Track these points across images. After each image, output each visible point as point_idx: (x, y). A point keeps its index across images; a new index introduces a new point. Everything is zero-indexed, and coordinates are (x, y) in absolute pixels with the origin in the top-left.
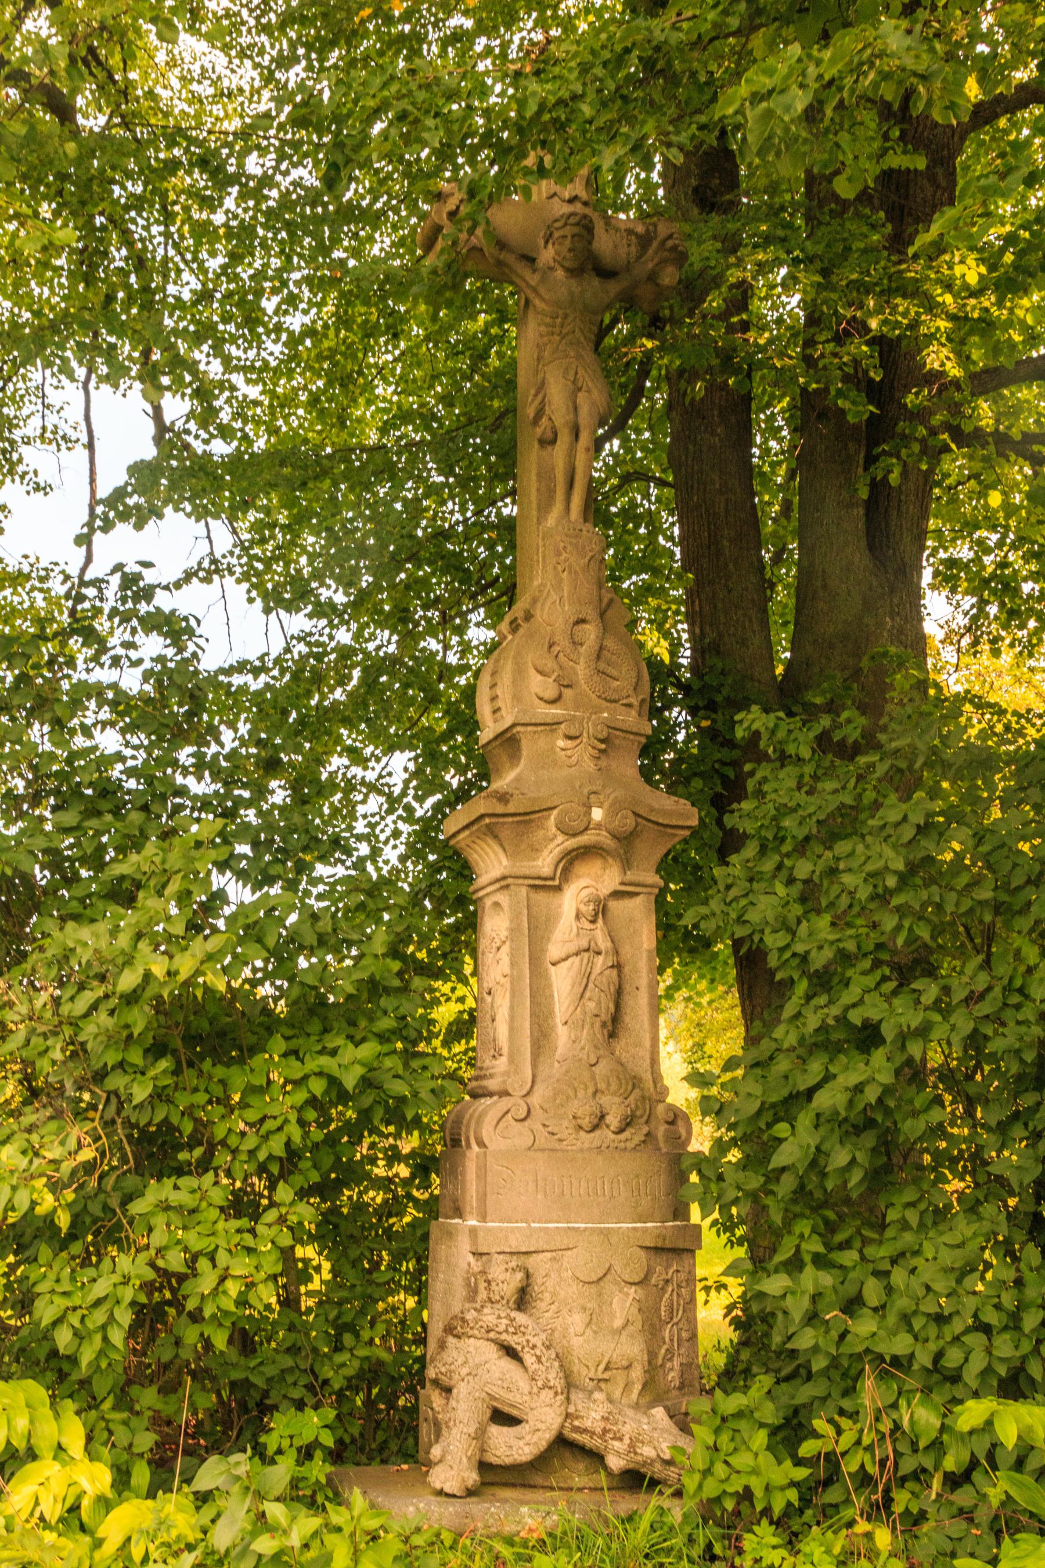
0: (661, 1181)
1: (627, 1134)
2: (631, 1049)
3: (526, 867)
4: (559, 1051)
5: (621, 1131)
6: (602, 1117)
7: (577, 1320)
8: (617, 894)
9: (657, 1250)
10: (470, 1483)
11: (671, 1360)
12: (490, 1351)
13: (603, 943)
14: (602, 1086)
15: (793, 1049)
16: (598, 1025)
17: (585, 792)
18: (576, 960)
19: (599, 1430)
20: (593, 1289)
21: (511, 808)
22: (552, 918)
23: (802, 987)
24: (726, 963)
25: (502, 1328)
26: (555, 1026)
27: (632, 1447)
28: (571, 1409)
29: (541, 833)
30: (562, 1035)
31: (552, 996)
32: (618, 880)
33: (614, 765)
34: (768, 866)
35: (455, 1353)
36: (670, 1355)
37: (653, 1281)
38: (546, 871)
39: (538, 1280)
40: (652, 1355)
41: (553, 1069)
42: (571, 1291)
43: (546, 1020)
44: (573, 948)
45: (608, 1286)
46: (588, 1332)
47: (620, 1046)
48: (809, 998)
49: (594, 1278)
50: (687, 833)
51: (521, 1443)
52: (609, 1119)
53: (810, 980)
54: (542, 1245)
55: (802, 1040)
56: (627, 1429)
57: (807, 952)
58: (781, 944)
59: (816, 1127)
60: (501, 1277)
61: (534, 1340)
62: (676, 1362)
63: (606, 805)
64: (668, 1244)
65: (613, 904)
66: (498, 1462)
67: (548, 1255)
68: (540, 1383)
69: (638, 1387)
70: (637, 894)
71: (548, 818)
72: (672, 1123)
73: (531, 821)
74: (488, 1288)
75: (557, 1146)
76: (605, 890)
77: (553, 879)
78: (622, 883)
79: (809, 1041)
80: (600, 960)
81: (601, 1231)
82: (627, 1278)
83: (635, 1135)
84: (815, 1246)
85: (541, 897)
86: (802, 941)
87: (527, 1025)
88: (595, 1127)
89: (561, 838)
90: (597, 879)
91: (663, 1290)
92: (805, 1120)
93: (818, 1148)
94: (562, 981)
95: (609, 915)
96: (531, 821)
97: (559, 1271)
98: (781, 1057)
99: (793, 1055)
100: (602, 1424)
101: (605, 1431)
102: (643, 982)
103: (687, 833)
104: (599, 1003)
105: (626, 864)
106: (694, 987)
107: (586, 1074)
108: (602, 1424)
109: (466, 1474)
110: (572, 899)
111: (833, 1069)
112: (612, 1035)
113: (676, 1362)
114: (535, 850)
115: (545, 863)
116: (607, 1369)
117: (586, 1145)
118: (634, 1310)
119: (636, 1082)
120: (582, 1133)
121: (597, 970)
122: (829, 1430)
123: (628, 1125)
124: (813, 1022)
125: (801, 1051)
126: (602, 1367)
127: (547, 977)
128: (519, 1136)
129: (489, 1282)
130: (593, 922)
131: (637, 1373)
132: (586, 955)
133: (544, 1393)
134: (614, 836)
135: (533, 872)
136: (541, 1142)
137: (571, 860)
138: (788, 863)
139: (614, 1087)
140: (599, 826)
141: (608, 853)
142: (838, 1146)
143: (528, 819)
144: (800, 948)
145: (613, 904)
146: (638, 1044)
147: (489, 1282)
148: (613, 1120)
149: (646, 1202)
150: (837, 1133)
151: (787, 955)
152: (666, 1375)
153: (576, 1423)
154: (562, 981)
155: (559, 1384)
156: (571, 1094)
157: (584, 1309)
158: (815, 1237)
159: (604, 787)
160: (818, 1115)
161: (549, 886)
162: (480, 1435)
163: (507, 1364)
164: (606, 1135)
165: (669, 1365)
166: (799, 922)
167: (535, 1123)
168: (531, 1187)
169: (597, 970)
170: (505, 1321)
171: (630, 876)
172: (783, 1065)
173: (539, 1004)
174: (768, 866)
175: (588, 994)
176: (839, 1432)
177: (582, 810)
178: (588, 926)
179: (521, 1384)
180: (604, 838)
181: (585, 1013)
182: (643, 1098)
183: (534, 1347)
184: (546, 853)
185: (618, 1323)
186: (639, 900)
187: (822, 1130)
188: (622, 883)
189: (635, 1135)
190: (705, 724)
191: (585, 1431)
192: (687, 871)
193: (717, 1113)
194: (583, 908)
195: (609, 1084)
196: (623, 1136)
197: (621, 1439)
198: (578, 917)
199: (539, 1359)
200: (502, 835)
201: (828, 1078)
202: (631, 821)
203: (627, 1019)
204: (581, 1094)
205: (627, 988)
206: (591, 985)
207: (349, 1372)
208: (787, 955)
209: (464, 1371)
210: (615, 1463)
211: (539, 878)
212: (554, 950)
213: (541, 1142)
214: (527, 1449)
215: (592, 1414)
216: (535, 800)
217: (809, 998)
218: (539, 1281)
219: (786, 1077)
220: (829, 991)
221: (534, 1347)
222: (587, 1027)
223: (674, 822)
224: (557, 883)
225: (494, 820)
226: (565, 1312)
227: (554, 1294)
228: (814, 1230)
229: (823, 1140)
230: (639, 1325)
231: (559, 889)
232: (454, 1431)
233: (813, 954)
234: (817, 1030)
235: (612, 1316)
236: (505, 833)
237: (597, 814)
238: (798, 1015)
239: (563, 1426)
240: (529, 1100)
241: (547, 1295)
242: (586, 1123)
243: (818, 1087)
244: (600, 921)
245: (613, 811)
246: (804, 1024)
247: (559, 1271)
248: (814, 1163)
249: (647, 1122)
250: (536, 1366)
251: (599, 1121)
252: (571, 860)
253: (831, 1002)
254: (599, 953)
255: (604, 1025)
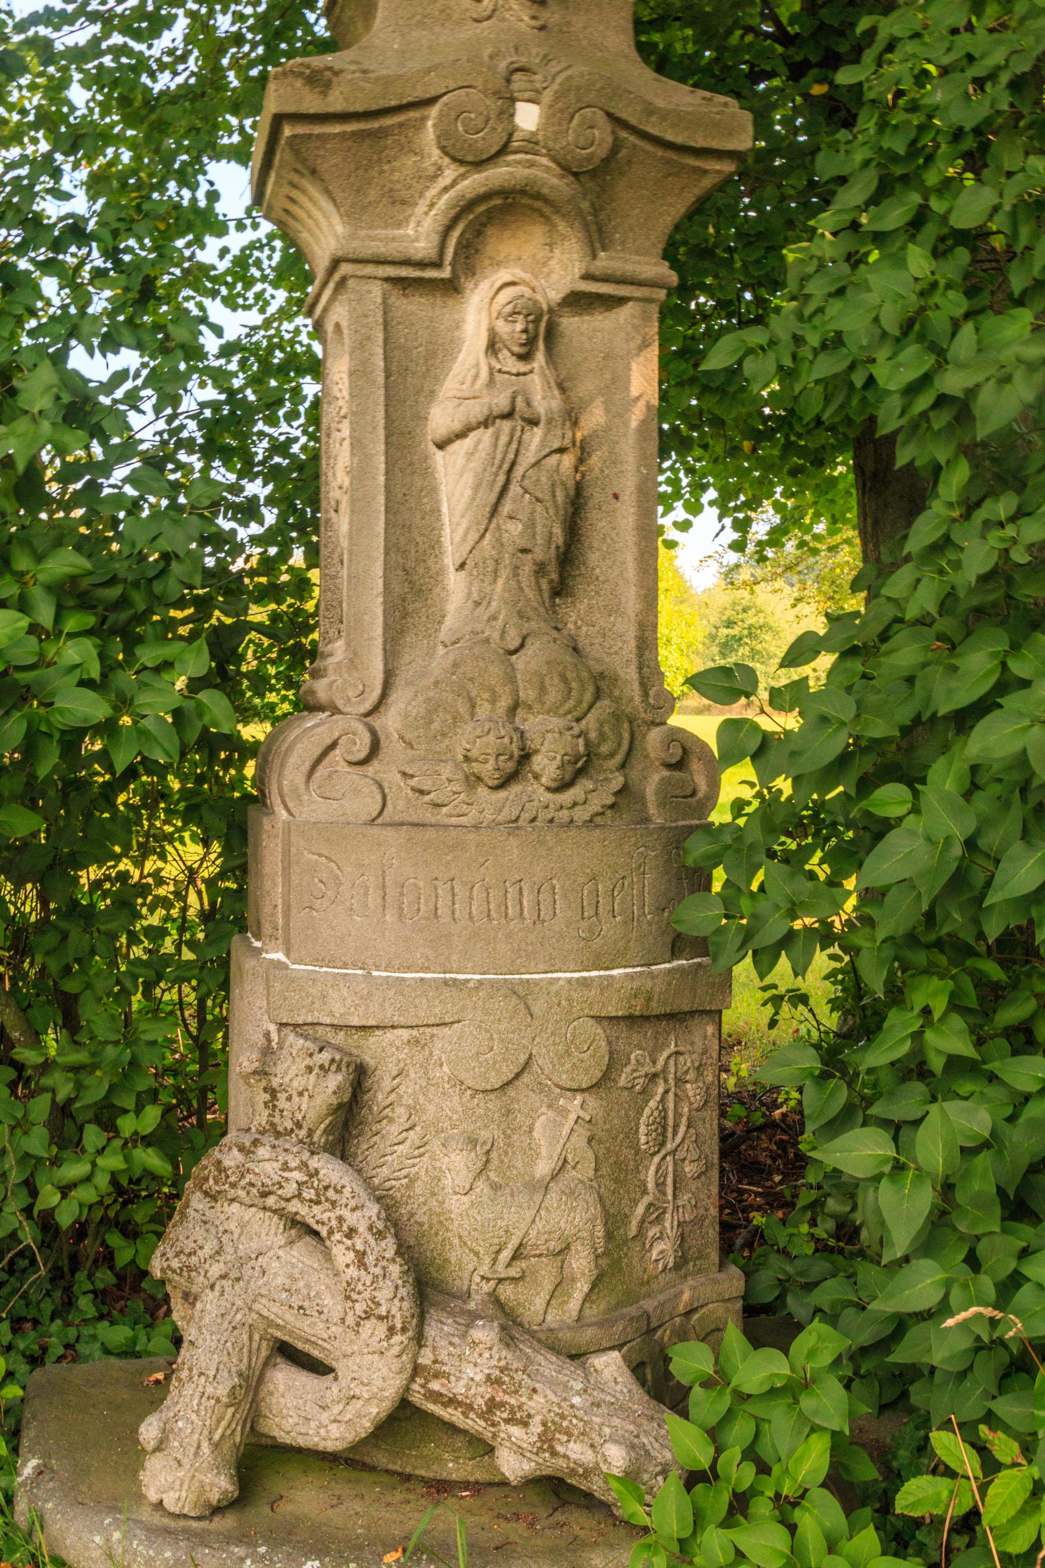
0: (650, 882)
1: (575, 793)
2: (600, 619)
3: (379, 240)
4: (449, 622)
5: (562, 786)
6: (525, 757)
7: (456, 1165)
8: (578, 301)
9: (631, 1020)
10: (214, 1497)
11: (659, 1220)
12: (268, 1232)
13: (543, 399)
14: (528, 694)
15: (923, 621)
16: (527, 570)
17: (502, 65)
18: (485, 436)
19: (480, 1402)
20: (494, 1103)
21: (336, 102)
22: (439, 353)
23: (957, 478)
24: (848, 493)
25: (291, 1189)
26: (441, 571)
27: (547, 1442)
28: (426, 1358)
29: (410, 161)
30: (456, 587)
31: (436, 511)
32: (578, 269)
33: (578, 22)
34: (895, 215)
35: (199, 1233)
36: (655, 1213)
37: (622, 1081)
38: (423, 246)
39: (382, 1085)
40: (613, 1222)
41: (431, 660)
42: (449, 1106)
43: (422, 560)
44: (476, 410)
45: (524, 1096)
46: (481, 1185)
47: (575, 614)
48: (970, 506)
49: (495, 1080)
50: (728, 167)
51: (325, 1417)
52: (538, 762)
53: (976, 465)
54: (390, 1015)
55: (948, 601)
56: (539, 1405)
57: (972, 393)
58: (911, 375)
59: (967, 795)
60: (297, 1084)
61: (352, 1219)
62: (669, 1223)
63: (547, 97)
64: (656, 1008)
65: (570, 323)
66: (288, 1440)
67: (405, 1034)
68: (360, 1308)
69: (582, 1287)
70: (621, 301)
71: (419, 125)
72: (680, 765)
73: (382, 133)
74: (271, 1104)
75: (429, 817)
76: (553, 292)
77: (438, 265)
78: (587, 277)
79: (967, 602)
80: (535, 438)
81: (512, 990)
82: (565, 1080)
83: (594, 794)
84: (951, 1040)
85: (415, 307)
86: (961, 366)
87: (378, 569)
88: (507, 781)
89: (451, 173)
90: (539, 267)
91: (646, 1093)
92: (944, 778)
93: (970, 844)
94: (456, 479)
95: (561, 348)
96: (382, 133)
97: (425, 1067)
98: (900, 636)
99: (931, 632)
100: (487, 1391)
101: (493, 1405)
102: (628, 485)
103: (728, 167)
104: (531, 525)
105: (597, 236)
106: (808, 529)
107: (495, 670)
108: (487, 1391)
109: (208, 1478)
110: (479, 312)
111: (1018, 668)
112: (561, 590)
113: (669, 1223)
114: (399, 202)
115: (419, 232)
116: (516, 1256)
117: (488, 816)
118: (580, 1141)
119: (601, 685)
120: (482, 791)
121: (529, 457)
122: (968, 1461)
123: (580, 773)
124: (977, 557)
125: (944, 625)
126: (506, 1255)
127: (427, 471)
128: (352, 796)
129: (273, 1093)
130: (524, 358)
131: (581, 1263)
132: (506, 426)
133: (368, 1326)
134: (567, 169)
135: (391, 250)
136: (398, 808)
137: (479, 223)
138: (937, 205)
139: (553, 695)
140: (532, 144)
141: (556, 208)
142: (1017, 847)
143: (378, 125)
144: (953, 382)
145: (570, 323)
146: (613, 610)
147: (273, 1093)
148: (546, 766)
149: (610, 929)
150: (1017, 811)
151: (923, 402)
152: (646, 1250)
153: (435, 1386)
154: (456, 479)
155: (400, 1309)
156: (463, 709)
157: (473, 1142)
158: (957, 1022)
159: (546, 60)
160: (974, 769)
161: (435, 280)
162: (250, 1391)
163: (301, 1255)
164: (534, 793)
165: (653, 1231)
166: (956, 326)
167: (382, 769)
168: (373, 899)
169: (529, 457)
170: (298, 1176)
171: (604, 262)
172: (905, 654)
173: (407, 528)
174: (895, 215)
175: (506, 508)
176: (991, 1466)
177: (494, 105)
178: (512, 365)
179: (327, 1301)
180: (543, 173)
181: (499, 544)
182: (617, 717)
183: (351, 1233)
184: (421, 208)
185: (543, 1168)
186: (625, 313)
187: (982, 802)
188: (587, 277)
189: (594, 794)
190: (818, 90)
191: (452, 1402)
192: (722, 257)
193: (755, 757)
194: (503, 328)
195: (542, 690)
196: (567, 797)
197: (525, 1424)
198: (493, 347)
199: (361, 1257)
200: (323, 167)
201: (1007, 684)
202: (602, 135)
203: (593, 558)
204: (483, 710)
205: (596, 495)
206: (515, 489)
207: (86, 1194)
208: (923, 402)
209: (216, 1270)
210: (512, 1465)
211: (406, 263)
212: (441, 418)
213: (398, 808)
214: (335, 1431)
215: (469, 1365)
216: (387, 82)
217: (970, 506)
218: (387, 1084)
219: (910, 680)
220: (1021, 486)
221: (351, 1233)
222: (504, 573)
223: (700, 143)
224: (446, 273)
225: (301, 129)
226: (435, 1145)
227: (412, 1111)
228: (955, 1006)
229: (984, 824)
230: (587, 1170)
231: (452, 288)
232: (188, 1391)
233: (986, 396)
234: (985, 579)
235: (532, 1153)
236: (330, 162)
237: (528, 117)
238: (944, 544)
239: (407, 1389)
240: (377, 722)
241: (400, 1111)
242: (488, 769)
243: (984, 707)
244: (540, 357)
245: (559, 114)
246: (957, 565)
247: (425, 1067)
248: (958, 880)
249: (623, 766)
250: (353, 1272)
251: (518, 767)
252: (479, 223)
253: (1020, 514)
254: (534, 422)
255: (540, 569)
